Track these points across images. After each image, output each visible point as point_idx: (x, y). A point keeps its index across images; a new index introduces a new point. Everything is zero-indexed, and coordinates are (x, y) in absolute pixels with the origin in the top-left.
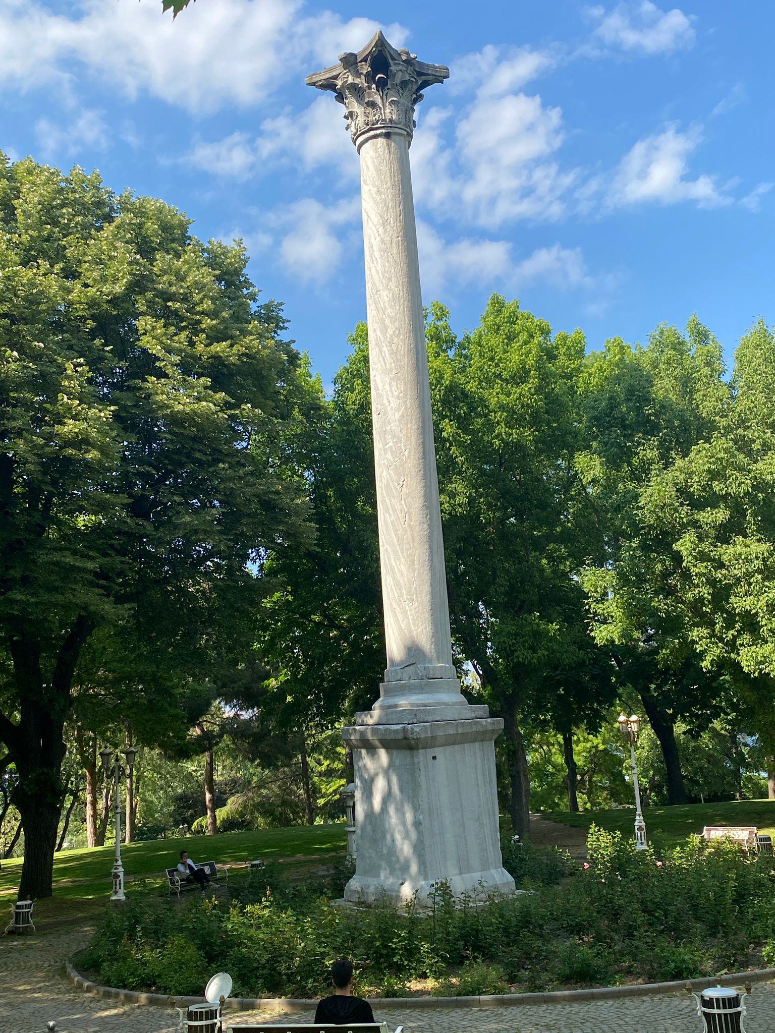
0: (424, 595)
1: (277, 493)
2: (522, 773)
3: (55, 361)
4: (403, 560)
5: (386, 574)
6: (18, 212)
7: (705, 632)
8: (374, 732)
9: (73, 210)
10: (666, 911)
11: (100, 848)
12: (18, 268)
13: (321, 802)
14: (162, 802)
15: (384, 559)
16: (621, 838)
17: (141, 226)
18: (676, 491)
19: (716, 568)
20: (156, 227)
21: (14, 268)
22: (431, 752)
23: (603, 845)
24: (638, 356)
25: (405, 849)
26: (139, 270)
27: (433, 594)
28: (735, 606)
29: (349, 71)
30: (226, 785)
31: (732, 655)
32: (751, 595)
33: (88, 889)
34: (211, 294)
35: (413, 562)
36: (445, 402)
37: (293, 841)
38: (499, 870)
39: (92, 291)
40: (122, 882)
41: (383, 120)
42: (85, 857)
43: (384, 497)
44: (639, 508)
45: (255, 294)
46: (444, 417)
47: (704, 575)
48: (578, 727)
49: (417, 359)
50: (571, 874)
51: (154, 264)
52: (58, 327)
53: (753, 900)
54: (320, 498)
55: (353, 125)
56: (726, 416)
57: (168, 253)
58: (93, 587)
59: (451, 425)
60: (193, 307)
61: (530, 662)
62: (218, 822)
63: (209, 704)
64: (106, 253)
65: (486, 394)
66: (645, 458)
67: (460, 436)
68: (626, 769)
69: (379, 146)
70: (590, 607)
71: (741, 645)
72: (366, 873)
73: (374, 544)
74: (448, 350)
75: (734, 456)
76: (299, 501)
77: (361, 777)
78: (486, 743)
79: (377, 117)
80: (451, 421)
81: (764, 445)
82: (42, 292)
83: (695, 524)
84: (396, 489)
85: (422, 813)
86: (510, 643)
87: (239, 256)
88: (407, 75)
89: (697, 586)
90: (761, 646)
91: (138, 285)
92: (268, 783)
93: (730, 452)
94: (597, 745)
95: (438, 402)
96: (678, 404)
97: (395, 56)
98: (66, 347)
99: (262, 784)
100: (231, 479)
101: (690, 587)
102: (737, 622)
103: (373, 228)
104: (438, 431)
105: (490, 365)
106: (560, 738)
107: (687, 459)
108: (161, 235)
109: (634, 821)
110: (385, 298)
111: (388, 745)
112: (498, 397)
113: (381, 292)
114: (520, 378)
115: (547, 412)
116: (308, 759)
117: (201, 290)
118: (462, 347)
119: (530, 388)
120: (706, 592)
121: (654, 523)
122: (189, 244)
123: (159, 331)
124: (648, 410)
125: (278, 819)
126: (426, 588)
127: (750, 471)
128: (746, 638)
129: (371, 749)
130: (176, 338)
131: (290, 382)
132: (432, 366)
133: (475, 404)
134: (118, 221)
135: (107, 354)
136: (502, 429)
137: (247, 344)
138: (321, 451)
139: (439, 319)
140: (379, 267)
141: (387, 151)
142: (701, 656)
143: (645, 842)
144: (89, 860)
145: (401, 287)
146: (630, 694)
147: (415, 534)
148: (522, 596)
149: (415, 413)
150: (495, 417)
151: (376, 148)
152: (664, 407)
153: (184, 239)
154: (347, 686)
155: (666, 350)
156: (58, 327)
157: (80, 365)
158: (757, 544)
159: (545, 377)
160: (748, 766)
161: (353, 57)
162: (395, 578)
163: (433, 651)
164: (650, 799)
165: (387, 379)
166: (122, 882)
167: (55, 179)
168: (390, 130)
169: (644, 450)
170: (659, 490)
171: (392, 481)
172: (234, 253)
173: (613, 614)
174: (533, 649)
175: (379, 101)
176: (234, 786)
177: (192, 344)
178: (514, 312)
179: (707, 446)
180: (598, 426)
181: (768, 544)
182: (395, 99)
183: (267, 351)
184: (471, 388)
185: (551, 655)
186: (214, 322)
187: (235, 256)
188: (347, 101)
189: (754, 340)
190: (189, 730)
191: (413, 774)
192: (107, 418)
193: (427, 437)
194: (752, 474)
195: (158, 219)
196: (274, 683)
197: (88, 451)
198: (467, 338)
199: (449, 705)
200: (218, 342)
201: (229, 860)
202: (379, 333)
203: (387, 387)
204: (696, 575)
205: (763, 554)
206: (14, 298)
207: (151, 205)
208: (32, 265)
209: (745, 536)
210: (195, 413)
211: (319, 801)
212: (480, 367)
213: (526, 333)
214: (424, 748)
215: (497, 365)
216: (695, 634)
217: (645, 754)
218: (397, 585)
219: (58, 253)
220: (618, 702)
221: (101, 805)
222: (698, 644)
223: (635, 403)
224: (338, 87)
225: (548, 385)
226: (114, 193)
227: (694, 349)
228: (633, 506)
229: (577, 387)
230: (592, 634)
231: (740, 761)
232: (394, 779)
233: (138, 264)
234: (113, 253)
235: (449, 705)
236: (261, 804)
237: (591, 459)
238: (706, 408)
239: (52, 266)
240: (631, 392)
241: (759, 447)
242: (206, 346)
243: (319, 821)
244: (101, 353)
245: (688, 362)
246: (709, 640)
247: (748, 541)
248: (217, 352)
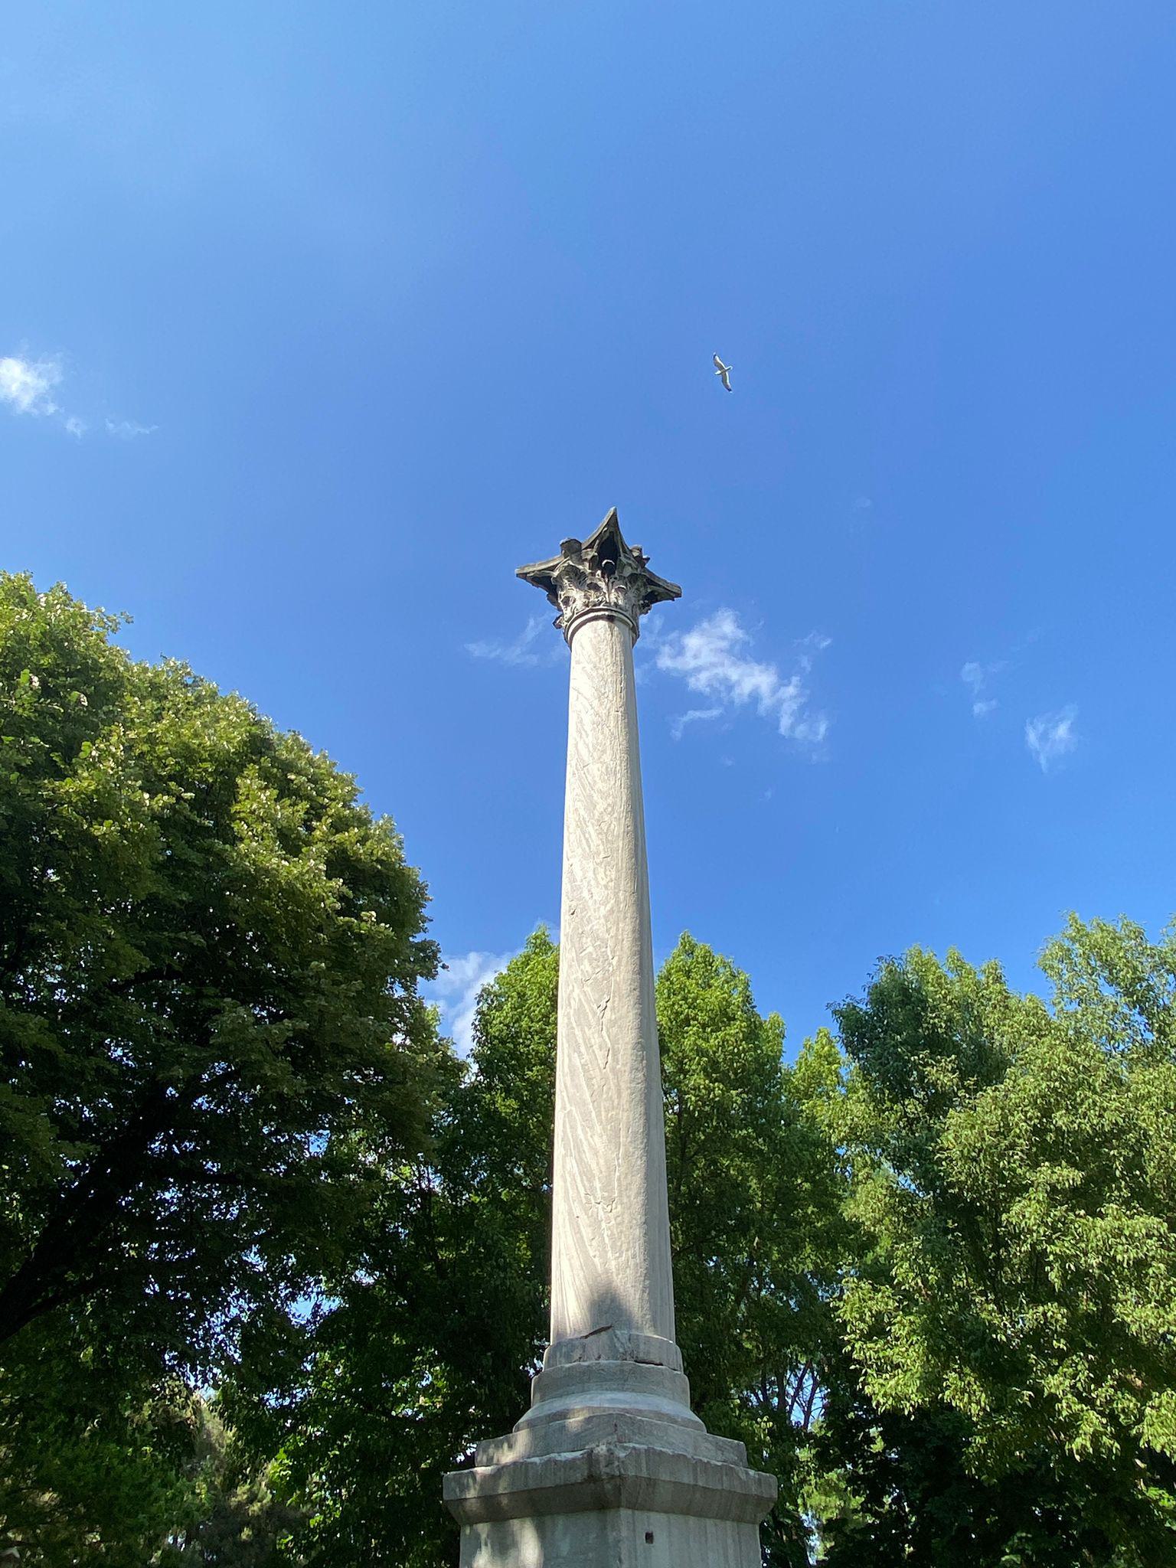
0: (633, 1194)
4: (598, 1128)
15: (564, 1132)
35: (616, 1133)
43: (573, 1028)
49: (636, 846)
78: (746, 1528)
79: (600, 599)
84: (595, 1014)
113: (590, 767)
126: (637, 1181)
136: (698, 1080)
141: (609, 632)
145: (618, 762)
147: (623, 1086)
162: (581, 1159)
168: (614, 614)
171: (588, 1001)
175: (602, 584)
199: (675, 1422)
202: (582, 812)
203: (590, 874)
214: (633, 1506)
218: (587, 1174)
230: (868, 1390)
235: (675, 1422)
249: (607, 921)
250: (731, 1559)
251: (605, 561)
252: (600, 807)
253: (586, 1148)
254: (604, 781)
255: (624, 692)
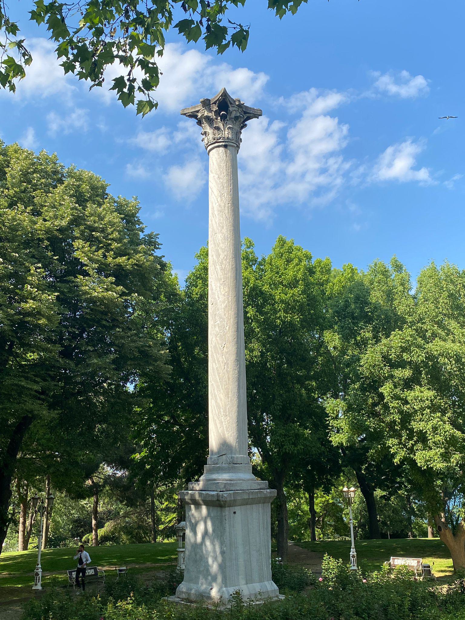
1: (150, 346)
2: (284, 519)
3: (24, 264)
4: (222, 391)
5: (212, 399)
6: (8, 175)
7: (396, 441)
8: (200, 495)
9: (40, 175)
10: (368, 614)
11: (26, 552)
12: (6, 210)
13: (161, 527)
14: (65, 522)
16: (342, 563)
17: (79, 186)
18: (382, 357)
19: (403, 404)
20: (88, 187)
21: (4, 210)
22: (233, 509)
23: (331, 567)
24: (362, 277)
25: (214, 568)
26: (77, 213)
27: (239, 412)
28: (414, 427)
29: (206, 109)
30: (104, 514)
31: (412, 456)
32: (423, 421)
33: (18, 580)
34: (118, 229)
36: (250, 296)
37: (144, 553)
38: (270, 582)
39: (48, 224)
40: (40, 578)
41: (223, 138)
42: (17, 558)
43: (213, 353)
44: (360, 366)
45: (143, 228)
46: (248, 305)
47: (396, 408)
48: (318, 490)
49: (236, 274)
50: (312, 584)
51: (86, 210)
52: (27, 244)
53: (420, 609)
54: (173, 348)
55: (206, 139)
56: (412, 315)
57: (95, 204)
58: (37, 399)
59: (252, 310)
60: (107, 236)
61: (292, 452)
62: (99, 537)
63: (98, 467)
64: (58, 201)
65: (273, 292)
66: (365, 337)
67: (258, 317)
68: (345, 514)
69: (220, 152)
70: (329, 422)
71: (417, 450)
72: (190, 580)
73: (204, 377)
74: (253, 266)
75: (416, 339)
76: (163, 352)
77: (190, 521)
78: (266, 504)
79: (220, 135)
80: (252, 307)
81: (433, 334)
82: (19, 224)
83: (392, 377)
84: (220, 349)
85: (226, 546)
86: (281, 440)
87: (135, 206)
88: (238, 113)
89: (393, 413)
90: (428, 451)
91: (76, 221)
92: (130, 515)
93: (413, 337)
94: (328, 500)
95: (246, 296)
96: (384, 306)
97: (232, 102)
98: (30, 256)
99: (126, 515)
100: (122, 338)
101: (388, 414)
102: (415, 436)
103: (215, 198)
104: (246, 313)
105: (276, 276)
106: (307, 495)
107: (388, 339)
108: (90, 192)
109: (350, 551)
110: (220, 237)
111: (209, 503)
112: (280, 295)
113: (218, 234)
114: (293, 284)
115: (308, 305)
116: (155, 501)
117: (113, 225)
118: (260, 264)
119: (299, 291)
120: (397, 417)
121: (369, 375)
122: (106, 198)
123: (86, 249)
124: (367, 309)
125: (135, 536)
126: (235, 408)
127: (424, 349)
128: (420, 445)
129: (197, 505)
130: (96, 253)
131: (161, 279)
132: (244, 275)
133: (267, 298)
134: (66, 183)
135: (55, 261)
136: (282, 314)
137: (137, 258)
138: (176, 320)
139: (249, 248)
140: (217, 220)
141: (225, 155)
142: (393, 456)
143: (356, 565)
144: (20, 560)
145: (229, 232)
146: (349, 470)
148: (289, 412)
149: (233, 306)
150: (278, 307)
151: (219, 153)
152: (376, 308)
153: (104, 195)
154: (182, 461)
155: (378, 275)
156: (27, 244)
157: (39, 268)
158: (427, 391)
159: (308, 285)
160: (416, 515)
161: (208, 101)
163: (237, 447)
164: (358, 533)
165: (218, 285)
166: (40, 578)
167: (31, 157)
169: (364, 332)
170: (372, 356)
171: (218, 344)
172: (132, 204)
173: (343, 427)
174: (295, 444)
176: (110, 515)
177: (105, 256)
178: (291, 247)
179: (400, 332)
180: (338, 317)
181: (434, 391)
182: (231, 126)
183: (149, 263)
184: (265, 289)
185: (305, 449)
186: (119, 245)
187: (133, 206)
188: (203, 125)
189: (428, 273)
190: (85, 482)
191: (221, 522)
192: (52, 300)
193: (240, 319)
194: (426, 351)
195: (89, 183)
196: (138, 456)
197: (39, 319)
198: (264, 259)
199: (245, 481)
200: (121, 257)
201: (105, 564)
202: (215, 257)
203: (218, 288)
204: (392, 408)
205: (431, 398)
206: (2, 227)
207: (86, 175)
208: (14, 208)
209: (421, 386)
210: (105, 298)
211: (160, 526)
212: (270, 277)
213: (297, 259)
214: (229, 506)
215: (280, 277)
216: (391, 442)
217: (356, 506)
218: (218, 406)
219: (30, 200)
220: (342, 474)
221: (28, 523)
222: (391, 448)
223: (360, 305)
224: (199, 117)
225: (309, 289)
226: (64, 167)
227: (394, 275)
228: (357, 365)
229: (326, 291)
230: (330, 439)
231: (412, 512)
232: (209, 524)
233: (77, 209)
234: (62, 202)
236: (125, 527)
237: (333, 335)
238: (401, 310)
239: (26, 208)
240: (357, 298)
241: (430, 335)
242: (113, 258)
243: (159, 539)
244: (51, 260)
245: (391, 283)
246: (398, 446)
247: (422, 389)
248: (119, 263)
249: (224, 311)
250: (261, 514)
251: (222, 112)
252: (222, 257)
253: (218, 398)
254: (223, 243)
255: (232, 191)
